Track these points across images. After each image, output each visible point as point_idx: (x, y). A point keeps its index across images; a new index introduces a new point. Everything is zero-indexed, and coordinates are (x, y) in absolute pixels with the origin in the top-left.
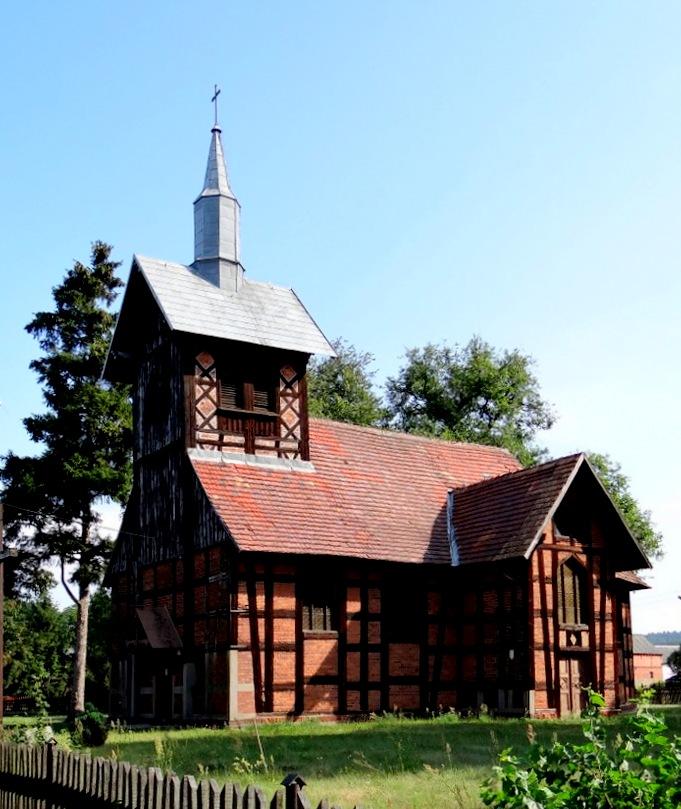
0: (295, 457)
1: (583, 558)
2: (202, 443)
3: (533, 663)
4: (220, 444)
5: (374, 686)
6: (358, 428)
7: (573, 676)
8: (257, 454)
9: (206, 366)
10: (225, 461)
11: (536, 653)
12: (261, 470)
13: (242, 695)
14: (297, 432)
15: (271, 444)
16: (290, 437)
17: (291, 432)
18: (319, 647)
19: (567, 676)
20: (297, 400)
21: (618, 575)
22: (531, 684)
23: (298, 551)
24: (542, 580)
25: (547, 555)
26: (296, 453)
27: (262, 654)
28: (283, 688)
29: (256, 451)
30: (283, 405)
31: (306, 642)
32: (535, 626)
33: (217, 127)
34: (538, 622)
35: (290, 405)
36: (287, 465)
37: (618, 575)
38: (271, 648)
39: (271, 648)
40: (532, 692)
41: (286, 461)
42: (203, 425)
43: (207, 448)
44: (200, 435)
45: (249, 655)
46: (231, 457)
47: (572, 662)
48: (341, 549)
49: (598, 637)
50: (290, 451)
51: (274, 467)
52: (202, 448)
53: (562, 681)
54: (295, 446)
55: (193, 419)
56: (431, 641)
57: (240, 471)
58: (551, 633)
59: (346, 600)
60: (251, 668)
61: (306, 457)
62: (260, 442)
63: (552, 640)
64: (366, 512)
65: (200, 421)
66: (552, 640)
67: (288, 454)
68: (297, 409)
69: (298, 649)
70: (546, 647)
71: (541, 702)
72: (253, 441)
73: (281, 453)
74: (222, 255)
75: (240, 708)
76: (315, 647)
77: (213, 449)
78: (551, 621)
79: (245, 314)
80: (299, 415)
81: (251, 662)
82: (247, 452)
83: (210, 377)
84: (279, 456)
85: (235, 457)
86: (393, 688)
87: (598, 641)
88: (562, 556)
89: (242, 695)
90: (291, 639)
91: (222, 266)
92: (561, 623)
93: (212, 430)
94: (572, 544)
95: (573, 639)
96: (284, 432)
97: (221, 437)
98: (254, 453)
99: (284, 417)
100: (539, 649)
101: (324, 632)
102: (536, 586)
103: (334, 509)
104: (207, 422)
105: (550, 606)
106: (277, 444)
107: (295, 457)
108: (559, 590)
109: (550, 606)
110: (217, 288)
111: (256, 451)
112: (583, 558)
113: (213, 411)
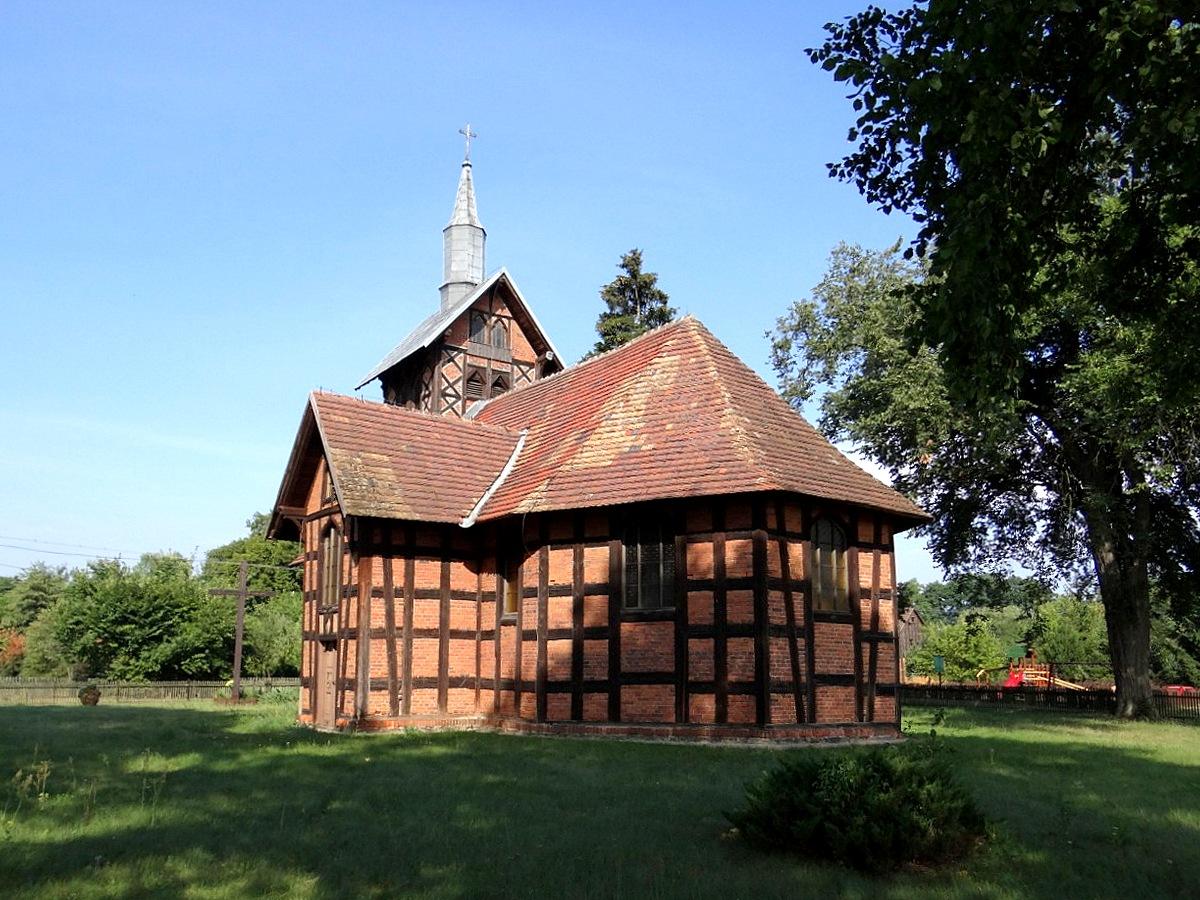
33: (466, 162)
59: (405, 558)
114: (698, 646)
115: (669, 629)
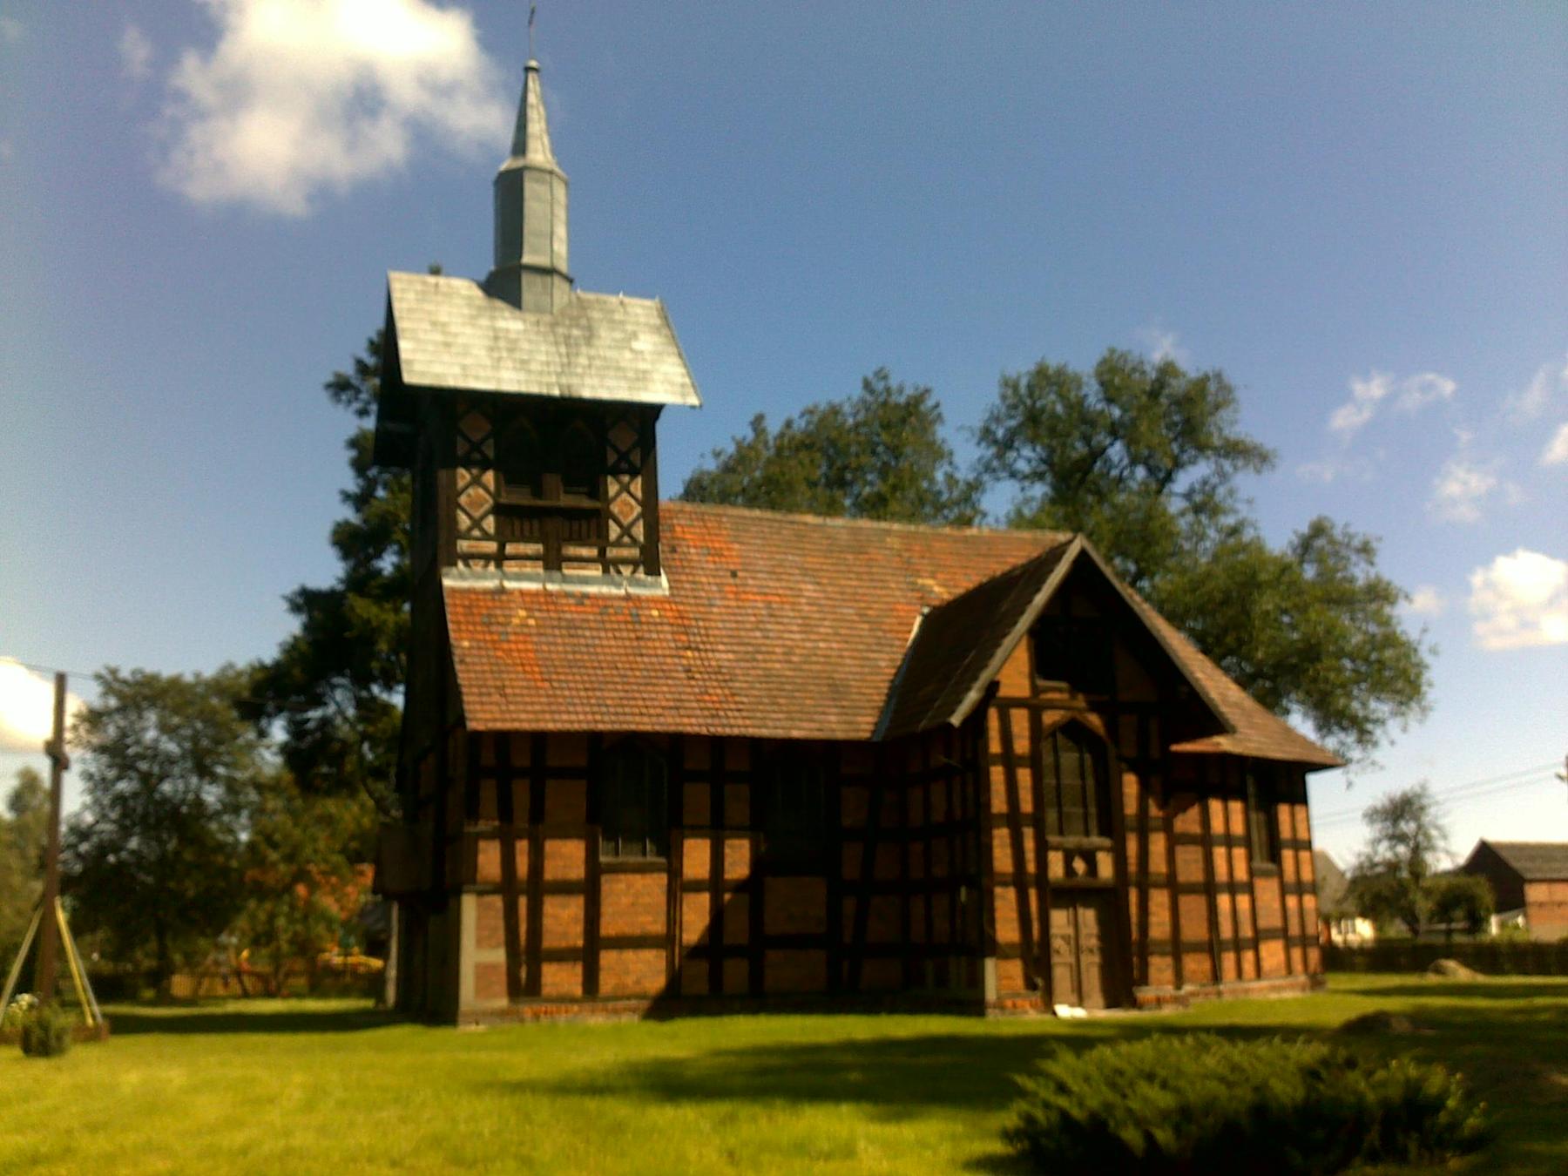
0: (634, 572)
1: (1094, 720)
2: (467, 558)
3: (992, 910)
4: (500, 558)
5: (736, 951)
6: (778, 516)
7: (1084, 931)
8: (566, 572)
9: (476, 437)
10: (509, 585)
11: (998, 890)
12: (568, 595)
13: (483, 971)
14: (639, 531)
15: (592, 552)
16: (626, 539)
17: (626, 531)
18: (629, 886)
19: (1070, 931)
20: (639, 480)
21: (1175, 748)
22: (987, 946)
23: (576, 726)
24: (1009, 761)
25: (1020, 721)
26: (635, 563)
27: (523, 902)
28: (560, 956)
29: (564, 565)
30: (613, 488)
31: (604, 878)
32: (996, 842)
34: (1001, 838)
35: (625, 488)
36: (619, 585)
37: (1175, 748)
38: (538, 888)
39: (538, 888)
40: (990, 965)
41: (617, 577)
42: (470, 529)
43: (478, 566)
44: (463, 545)
45: (497, 901)
46: (519, 577)
47: (1081, 911)
48: (662, 720)
49: (523, 928)
50: (625, 562)
51: (592, 589)
52: (467, 565)
53: (1057, 943)
54: (635, 552)
55: (454, 521)
56: (851, 869)
57: (528, 599)
58: (1030, 855)
60: (501, 924)
61: (653, 570)
62: (572, 551)
63: (1031, 867)
64: (740, 656)
65: (464, 521)
66: (1031, 867)
67: (622, 568)
68: (639, 494)
69: (590, 890)
70: (1019, 880)
71: (1010, 978)
72: (559, 550)
73: (607, 564)
74: (527, 259)
75: (482, 990)
76: (622, 886)
77: (486, 566)
78: (1028, 834)
79: (553, 349)
80: (459, 506)
81: (501, 914)
82: (547, 567)
83: (481, 452)
84: (606, 571)
85: (525, 580)
86: (773, 956)
87: (1132, 867)
88: (1050, 718)
89: (483, 971)
90: (577, 872)
91: (527, 279)
92: (1053, 839)
93: (486, 537)
94: (1073, 697)
95: (1079, 865)
96: (614, 531)
97: (502, 547)
98: (559, 569)
99: (615, 508)
100: (1005, 884)
101: (640, 859)
102: (997, 774)
103: (682, 653)
104: (477, 523)
105: (1027, 805)
106: (602, 552)
107: (634, 572)
108: (1049, 781)
109: (1027, 805)
110: (517, 313)
111: (564, 565)
112: (1094, 720)
113: (487, 507)
114: (1292, 901)
115: (662, 879)
